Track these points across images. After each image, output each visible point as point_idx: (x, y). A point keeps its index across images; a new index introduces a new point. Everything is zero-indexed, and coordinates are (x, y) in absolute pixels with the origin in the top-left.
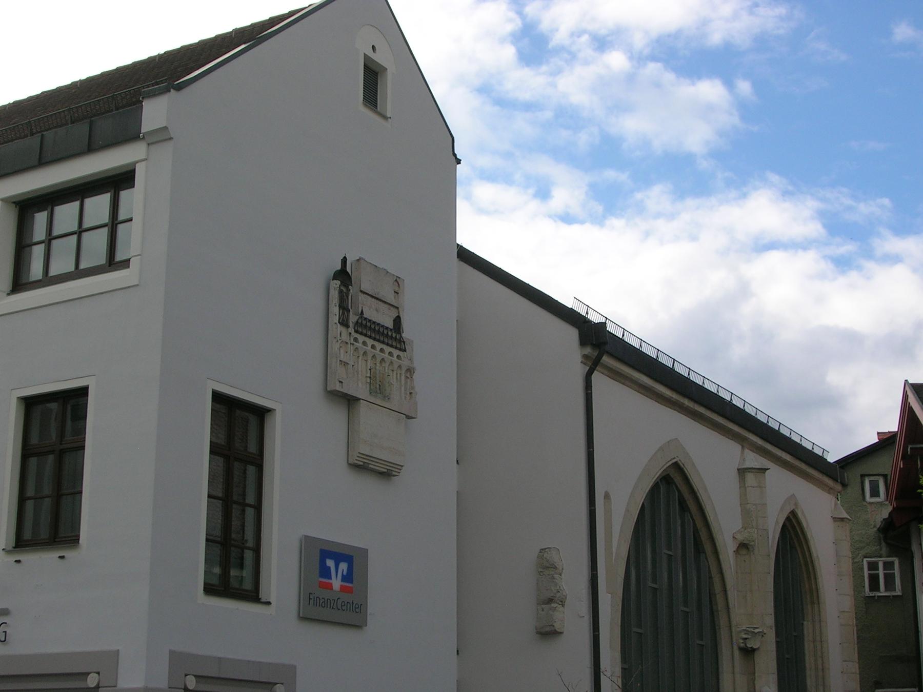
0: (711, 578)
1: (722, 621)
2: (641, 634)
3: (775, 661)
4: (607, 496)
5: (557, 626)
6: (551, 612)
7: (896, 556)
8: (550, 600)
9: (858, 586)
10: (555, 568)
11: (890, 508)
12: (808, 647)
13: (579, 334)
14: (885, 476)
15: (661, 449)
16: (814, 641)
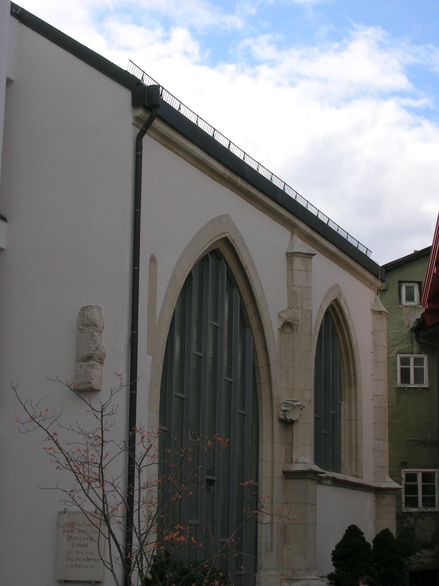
0: (255, 352)
1: (264, 394)
2: (183, 399)
3: (313, 434)
4: (153, 260)
5: (95, 384)
6: (89, 370)
7: (425, 354)
8: (89, 358)
9: (391, 378)
10: (96, 326)
11: (423, 310)
12: (344, 425)
13: (132, 94)
14: (420, 283)
15: (212, 222)
16: (350, 420)
